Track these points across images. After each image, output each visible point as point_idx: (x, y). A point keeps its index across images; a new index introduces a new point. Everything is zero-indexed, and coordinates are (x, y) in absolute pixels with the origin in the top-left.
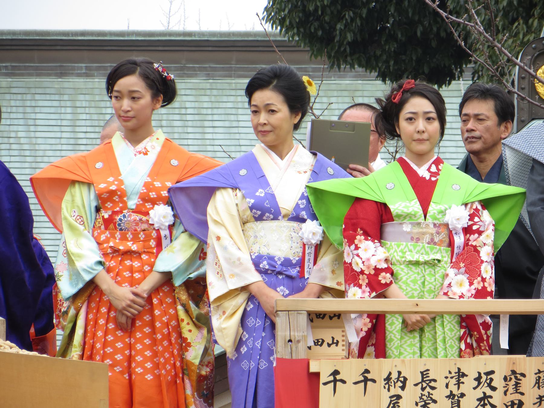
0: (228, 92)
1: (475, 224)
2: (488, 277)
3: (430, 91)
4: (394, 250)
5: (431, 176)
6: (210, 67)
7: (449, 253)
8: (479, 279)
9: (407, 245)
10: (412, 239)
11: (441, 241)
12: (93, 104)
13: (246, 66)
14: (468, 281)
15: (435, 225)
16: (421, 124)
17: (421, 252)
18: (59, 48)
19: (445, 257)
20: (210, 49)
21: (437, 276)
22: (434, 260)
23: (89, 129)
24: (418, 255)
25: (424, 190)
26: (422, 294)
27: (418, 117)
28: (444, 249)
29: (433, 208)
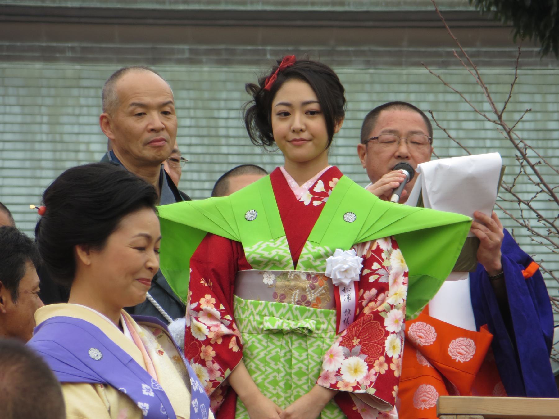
0: (396, 88)
1: (373, 273)
2: (396, 356)
3: (315, 72)
4: (250, 311)
5: (313, 199)
6: (370, 51)
7: (334, 318)
8: (382, 359)
9: (266, 306)
10: (275, 296)
11: (318, 299)
12: (200, 104)
13: (423, 49)
14: (366, 364)
15: (309, 276)
16: (298, 120)
17: (287, 316)
18: (151, 21)
19: (323, 323)
20: (371, 24)
21: (310, 351)
22: (304, 328)
23: (194, 140)
24: (281, 321)
25: (298, 221)
26: (288, 377)
27: (293, 111)
28: (321, 312)
29: (309, 250)
